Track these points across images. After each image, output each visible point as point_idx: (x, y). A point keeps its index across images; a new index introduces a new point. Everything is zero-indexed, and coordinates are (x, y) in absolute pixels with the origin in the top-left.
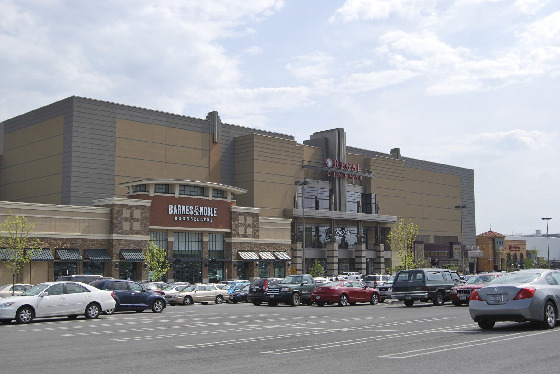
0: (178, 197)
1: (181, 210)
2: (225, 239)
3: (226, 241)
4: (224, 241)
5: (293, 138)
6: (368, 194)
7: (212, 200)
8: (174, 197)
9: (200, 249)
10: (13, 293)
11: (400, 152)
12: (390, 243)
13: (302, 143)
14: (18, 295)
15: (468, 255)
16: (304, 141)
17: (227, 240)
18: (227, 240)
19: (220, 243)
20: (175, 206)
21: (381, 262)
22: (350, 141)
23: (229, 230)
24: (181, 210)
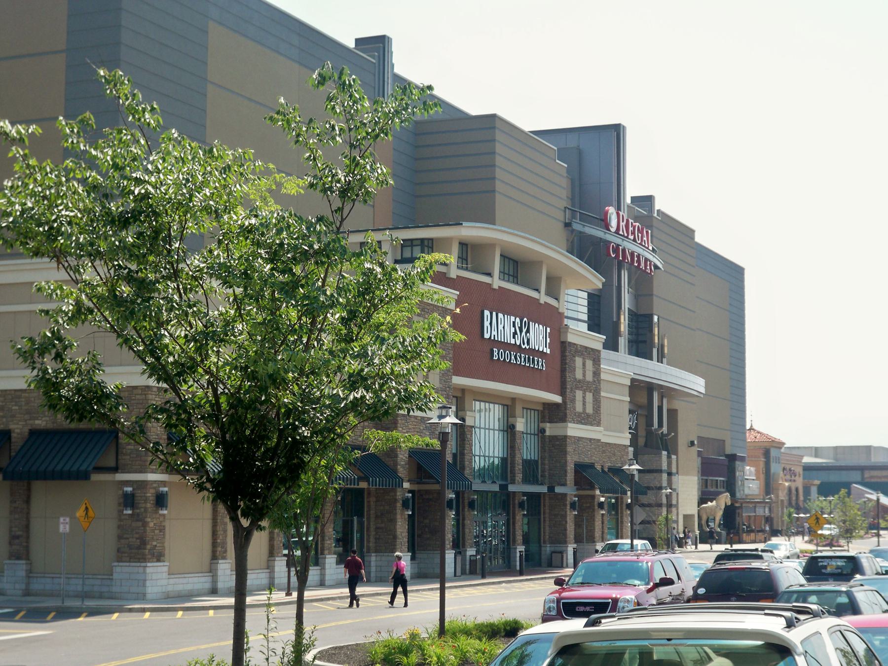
0: (455, 277)
1: (504, 328)
2: (542, 425)
3: (548, 433)
4: (543, 431)
5: (693, 231)
6: (641, 315)
7: (457, 276)
8: (490, 285)
9: (505, 456)
10: (632, 544)
11: (393, 65)
12: (363, 448)
13: (351, 45)
14: (663, 554)
15: (248, 581)
16: (358, 41)
17: (551, 429)
18: (551, 429)
19: (496, 432)
20: (494, 314)
21: (149, 590)
22: (658, 205)
23: (558, 399)
24: (504, 328)
